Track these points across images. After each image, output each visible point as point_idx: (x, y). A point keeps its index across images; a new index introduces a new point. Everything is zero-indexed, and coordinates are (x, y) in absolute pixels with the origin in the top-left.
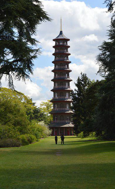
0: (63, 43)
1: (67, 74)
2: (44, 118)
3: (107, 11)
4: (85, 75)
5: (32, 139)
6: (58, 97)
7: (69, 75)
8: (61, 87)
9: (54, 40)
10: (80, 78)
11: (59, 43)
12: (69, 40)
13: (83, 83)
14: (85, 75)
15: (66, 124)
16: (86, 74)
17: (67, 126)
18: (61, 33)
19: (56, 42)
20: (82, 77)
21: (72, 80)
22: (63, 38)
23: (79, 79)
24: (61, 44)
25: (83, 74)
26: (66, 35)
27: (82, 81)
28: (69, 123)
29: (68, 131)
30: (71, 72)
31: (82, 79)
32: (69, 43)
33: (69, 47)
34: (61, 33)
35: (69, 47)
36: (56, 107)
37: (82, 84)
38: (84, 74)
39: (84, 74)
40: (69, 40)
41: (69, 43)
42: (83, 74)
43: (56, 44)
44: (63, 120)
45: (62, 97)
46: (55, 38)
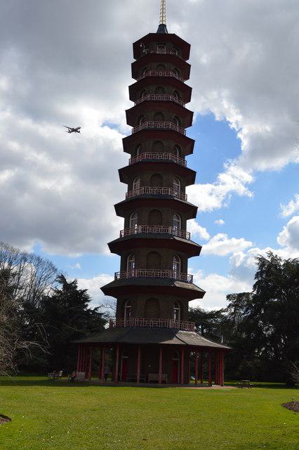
8: (153, 191)
18: (162, 27)
34: (162, 27)
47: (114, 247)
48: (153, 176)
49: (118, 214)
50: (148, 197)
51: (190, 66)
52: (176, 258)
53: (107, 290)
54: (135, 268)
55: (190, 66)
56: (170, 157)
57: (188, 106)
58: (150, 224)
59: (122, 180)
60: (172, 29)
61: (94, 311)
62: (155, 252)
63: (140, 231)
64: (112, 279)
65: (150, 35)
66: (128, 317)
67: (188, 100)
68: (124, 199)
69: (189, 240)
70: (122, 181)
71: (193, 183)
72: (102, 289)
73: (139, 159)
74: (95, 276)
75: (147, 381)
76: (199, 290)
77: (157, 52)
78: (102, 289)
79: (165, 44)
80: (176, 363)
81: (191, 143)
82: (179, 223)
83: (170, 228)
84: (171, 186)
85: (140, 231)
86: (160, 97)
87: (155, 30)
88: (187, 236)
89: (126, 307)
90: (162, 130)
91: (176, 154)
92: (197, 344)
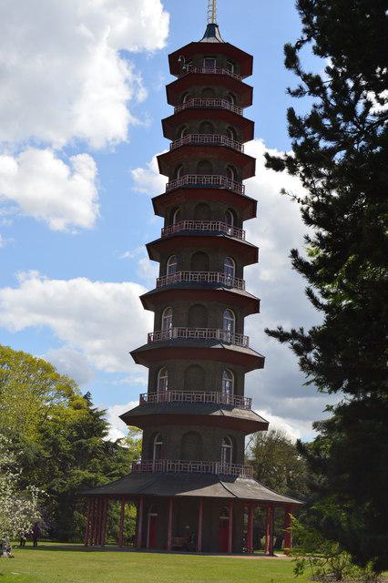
2: (120, 460)
6: (176, 330)
8: (196, 276)
15: (212, 480)
17: (217, 495)
18: (211, 29)
28: (231, 479)
34: (211, 29)
36: (162, 390)
44: (205, 325)
45: (199, 333)
47: (138, 356)
48: (204, 90)
49: (146, 307)
50: (186, 287)
51: (251, 89)
52: (228, 372)
53: (128, 418)
54: (173, 326)
55: (251, 89)
56: (225, 141)
57: (247, 113)
58: (190, 325)
59: (152, 258)
60: (225, 36)
61: (115, 444)
62: (196, 366)
63: (175, 336)
64: (137, 404)
65: (193, 44)
66: (159, 456)
67: (249, 102)
68: (159, 236)
69: (246, 347)
70: (151, 258)
71: (252, 138)
72: (131, 353)
73: (176, 228)
74: (117, 391)
75: (187, 547)
76: (260, 420)
77: (204, 71)
78: (131, 353)
79: (214, 57)
80: (226, 522)
81: (251, 124)
83: (218, 332)
84: (221, 269)
85: (175, 336)
86: (207, 139)
87: (198, 36)
88: (245, 342)
90: (209, 188)
91: (230, 136)
92: (260, 497)
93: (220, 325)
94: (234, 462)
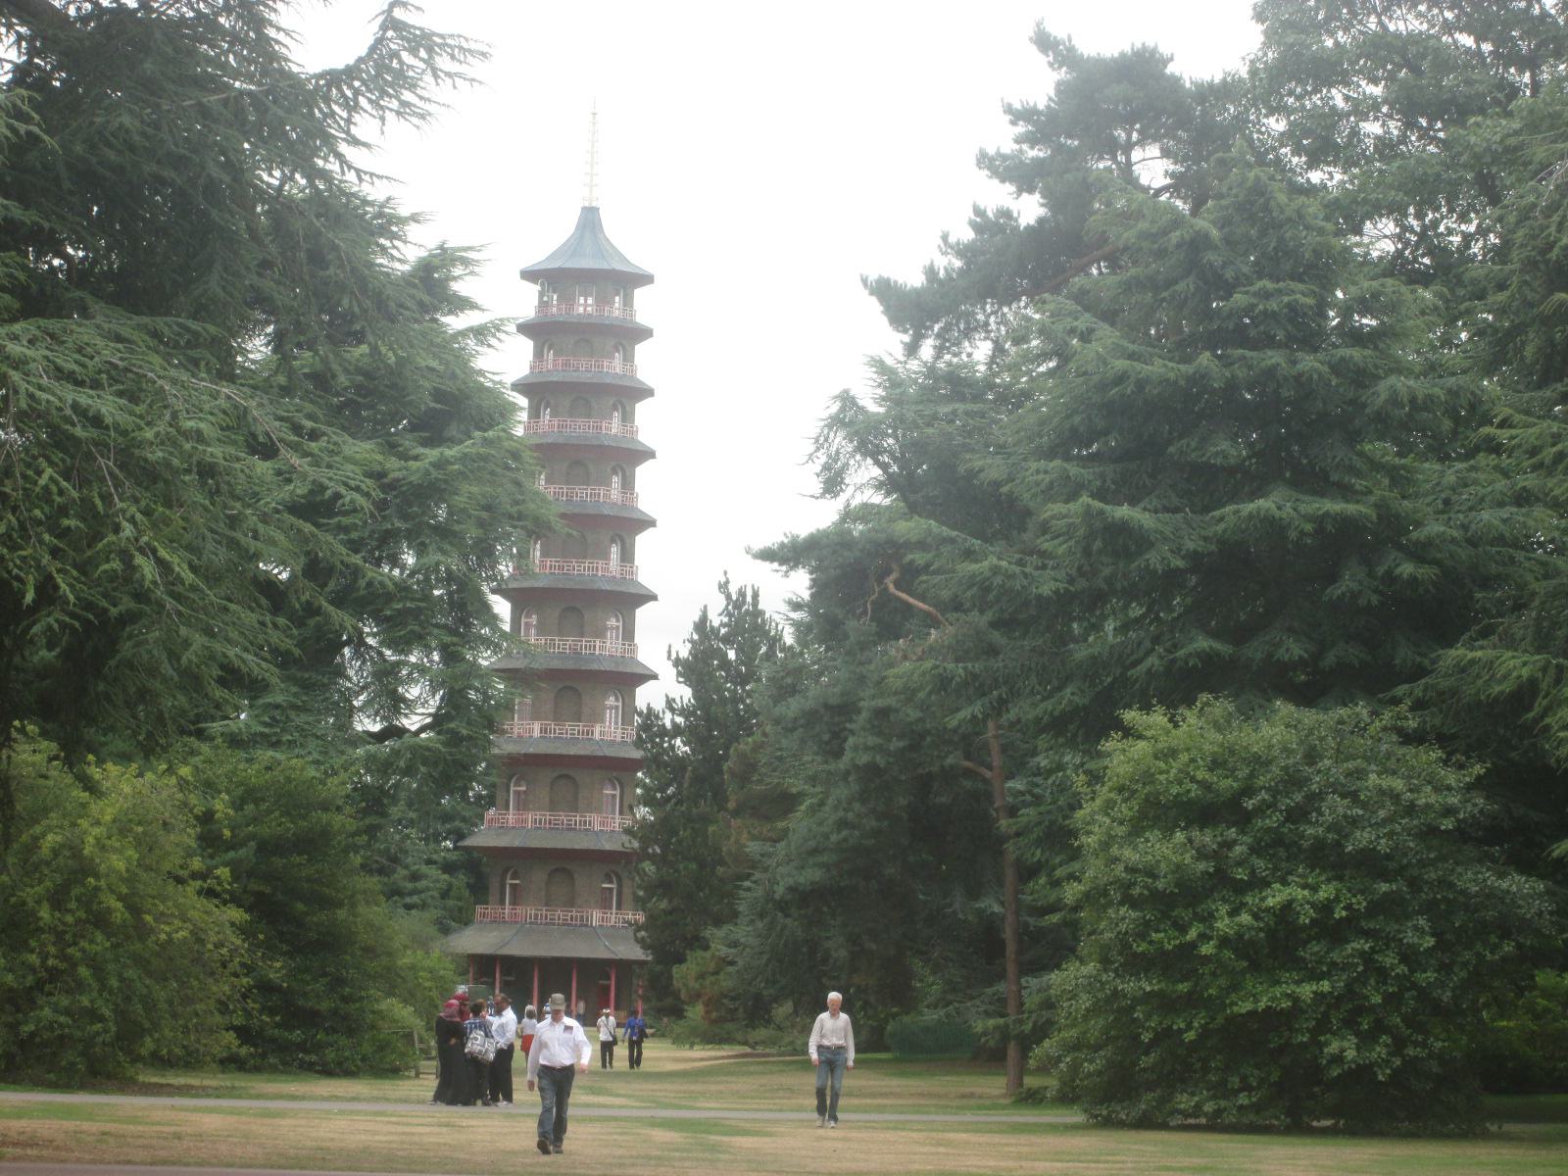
0: (603, 301)
1: (615, 479)
3: (952, 240)
4: (749, 599)
5: (367, 375)
7: (632, 632)
9: (529, 275)
10: (716, 620)
11: (568, 300)
12: (645, 279)
13: (732, 655)
14: (749, 599)
16: (756, 596)
18: (590, 219)
19: (541, 294)
20: (730, 615)
21: (655, 677)
22: (605, 266)
23: (701, 625)
24: (585, 305)
25: (733, 589)
26: (629, 241)
27: (727, 640)
29: (608, 987)
30: (649, 400)
31: (723, 631)
32: (645, 306)
33: (644, 333)
34: (590, 219)
35: (644, 333)
37: (725, 663)
38: (742, 594)
39: (742, 594)
40: (645, 279)
41: (645, 306)
42: (733, 589)
43: (543, 305)
44: (571, 903)
45: (570, 729)
46: (538, 254)
58: (558, 718)
62: (564, 870)
82: (617, 707)
89: (509, 881)
93: (606, 556)
94: (619, 907)
